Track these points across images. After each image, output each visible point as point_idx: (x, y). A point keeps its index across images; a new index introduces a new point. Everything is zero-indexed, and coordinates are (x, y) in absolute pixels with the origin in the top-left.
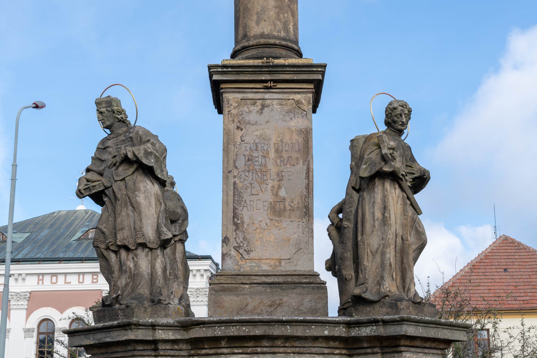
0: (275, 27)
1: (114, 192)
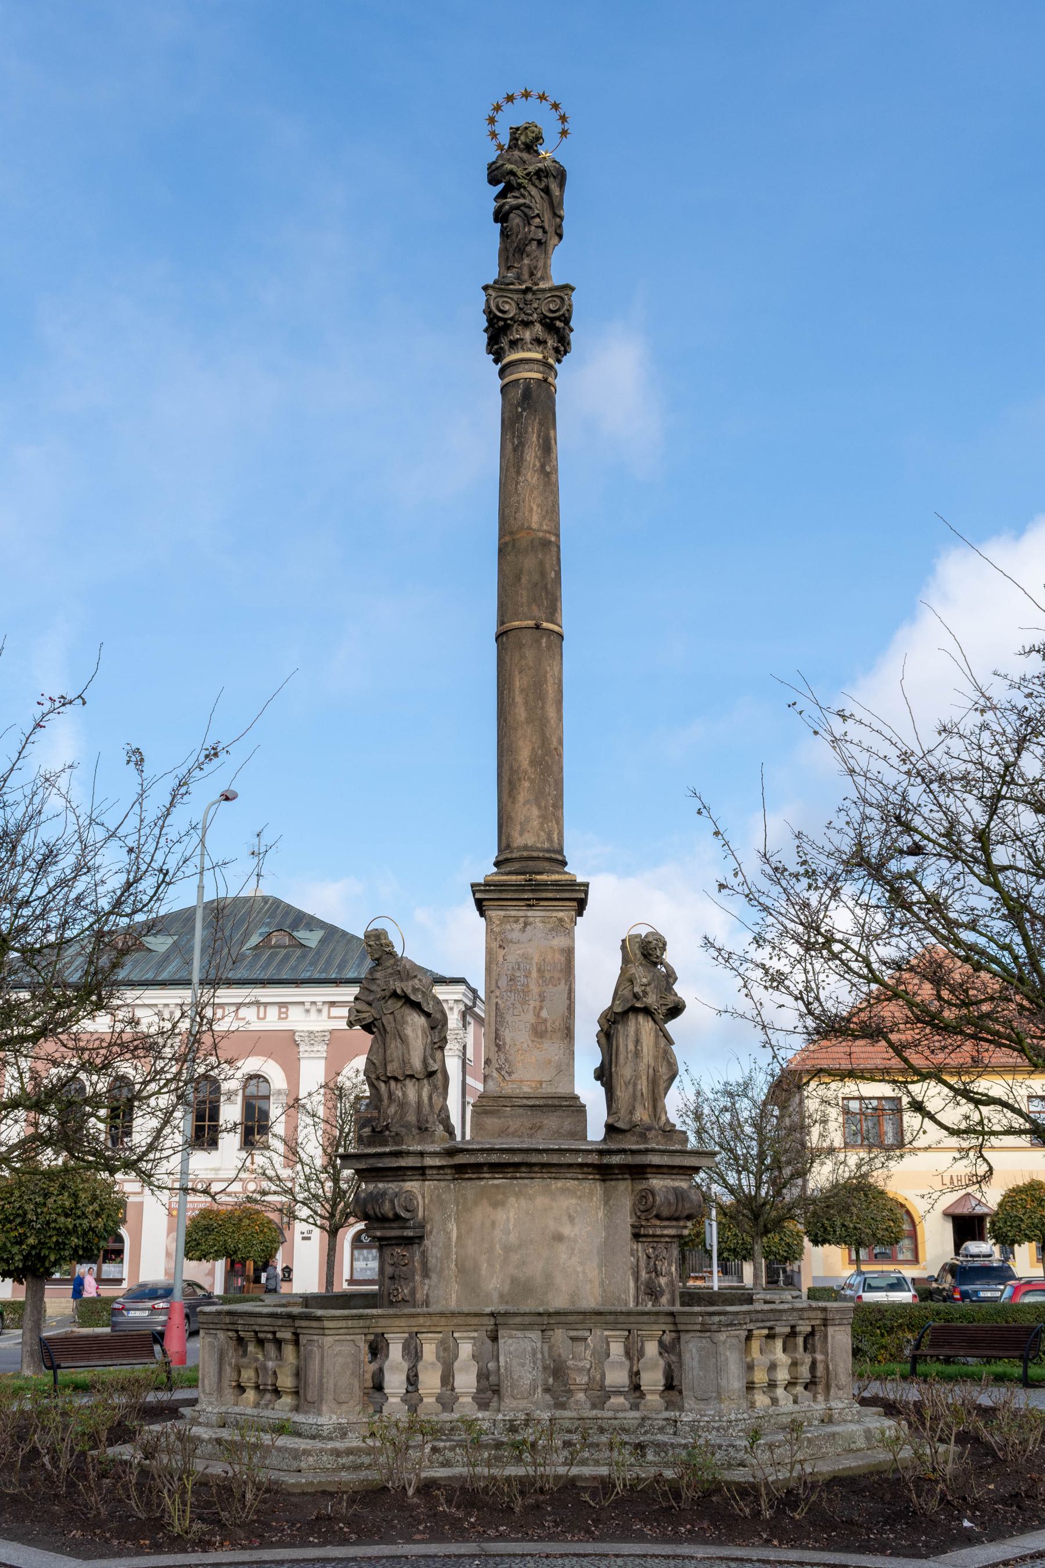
1: (383, 1025)
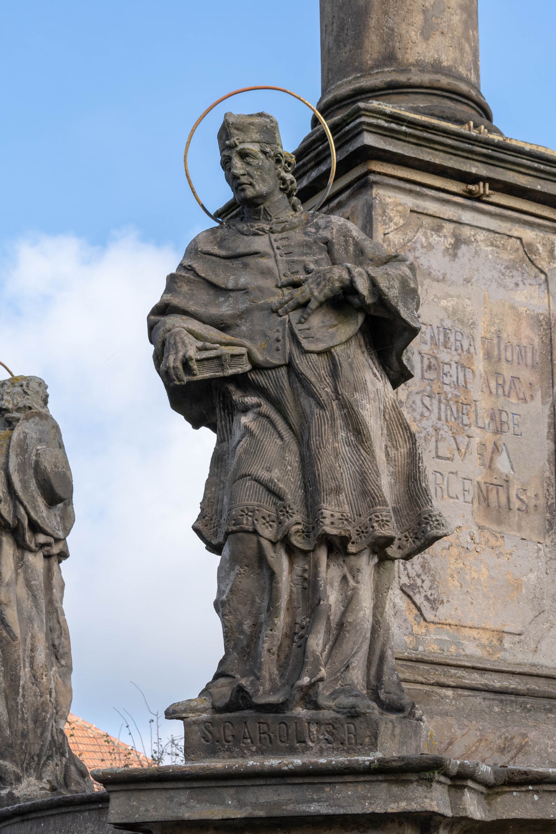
0: (462, 56)
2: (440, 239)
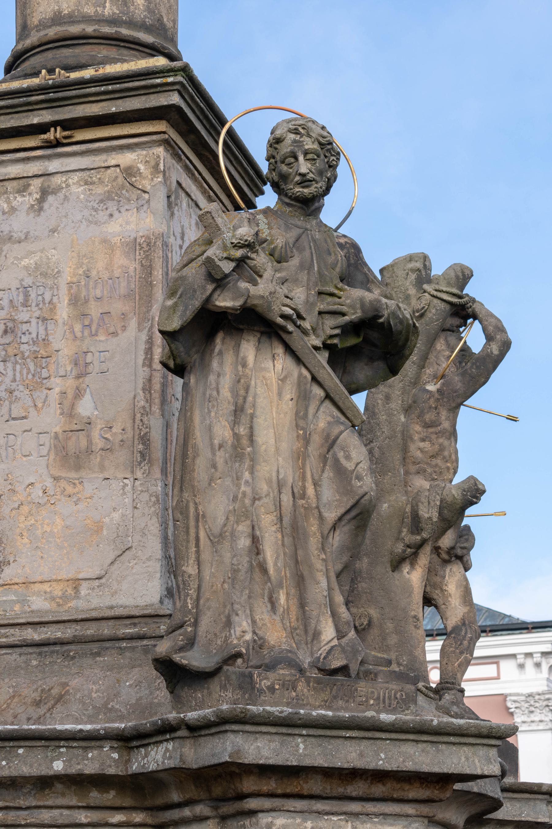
2: (25, 198)
